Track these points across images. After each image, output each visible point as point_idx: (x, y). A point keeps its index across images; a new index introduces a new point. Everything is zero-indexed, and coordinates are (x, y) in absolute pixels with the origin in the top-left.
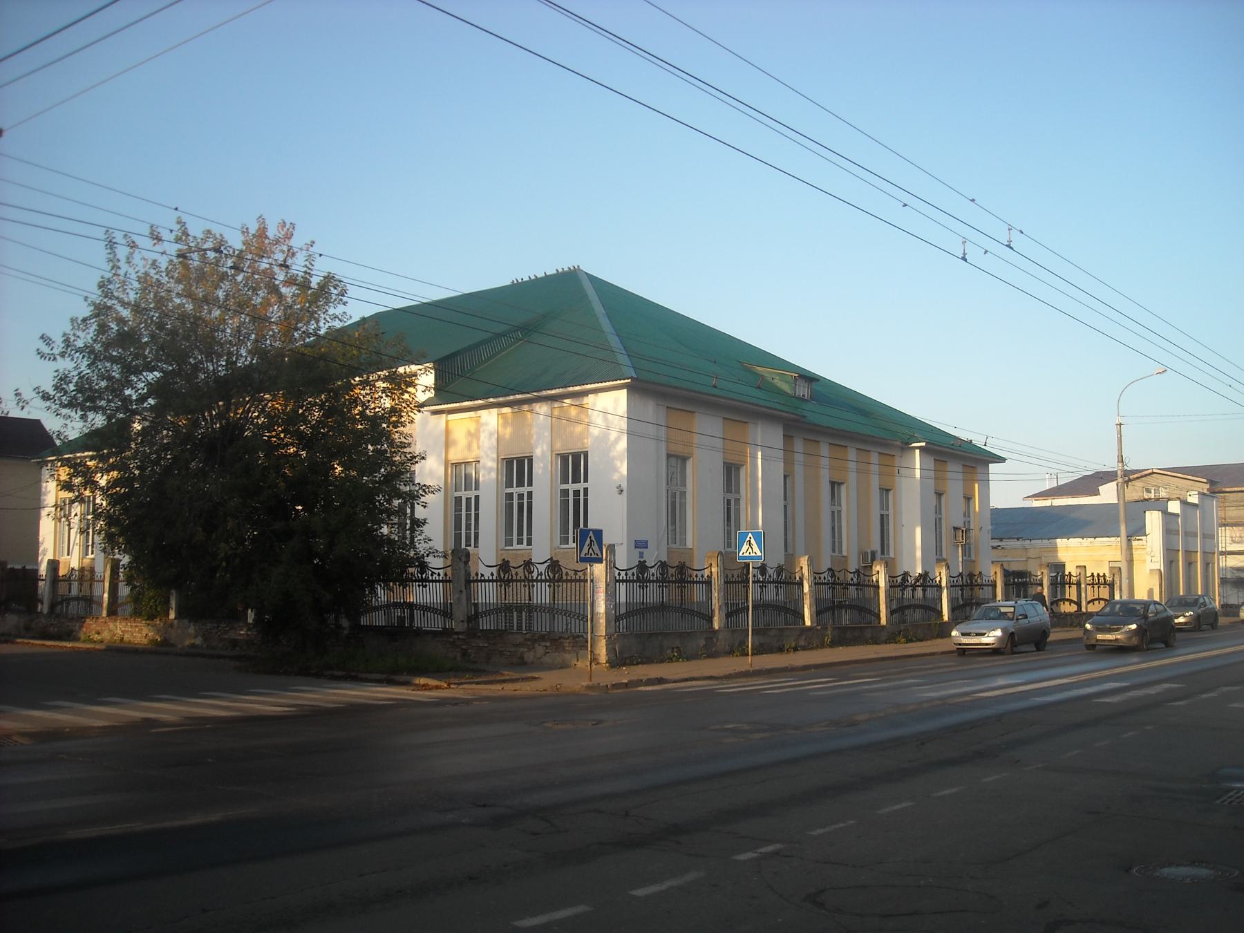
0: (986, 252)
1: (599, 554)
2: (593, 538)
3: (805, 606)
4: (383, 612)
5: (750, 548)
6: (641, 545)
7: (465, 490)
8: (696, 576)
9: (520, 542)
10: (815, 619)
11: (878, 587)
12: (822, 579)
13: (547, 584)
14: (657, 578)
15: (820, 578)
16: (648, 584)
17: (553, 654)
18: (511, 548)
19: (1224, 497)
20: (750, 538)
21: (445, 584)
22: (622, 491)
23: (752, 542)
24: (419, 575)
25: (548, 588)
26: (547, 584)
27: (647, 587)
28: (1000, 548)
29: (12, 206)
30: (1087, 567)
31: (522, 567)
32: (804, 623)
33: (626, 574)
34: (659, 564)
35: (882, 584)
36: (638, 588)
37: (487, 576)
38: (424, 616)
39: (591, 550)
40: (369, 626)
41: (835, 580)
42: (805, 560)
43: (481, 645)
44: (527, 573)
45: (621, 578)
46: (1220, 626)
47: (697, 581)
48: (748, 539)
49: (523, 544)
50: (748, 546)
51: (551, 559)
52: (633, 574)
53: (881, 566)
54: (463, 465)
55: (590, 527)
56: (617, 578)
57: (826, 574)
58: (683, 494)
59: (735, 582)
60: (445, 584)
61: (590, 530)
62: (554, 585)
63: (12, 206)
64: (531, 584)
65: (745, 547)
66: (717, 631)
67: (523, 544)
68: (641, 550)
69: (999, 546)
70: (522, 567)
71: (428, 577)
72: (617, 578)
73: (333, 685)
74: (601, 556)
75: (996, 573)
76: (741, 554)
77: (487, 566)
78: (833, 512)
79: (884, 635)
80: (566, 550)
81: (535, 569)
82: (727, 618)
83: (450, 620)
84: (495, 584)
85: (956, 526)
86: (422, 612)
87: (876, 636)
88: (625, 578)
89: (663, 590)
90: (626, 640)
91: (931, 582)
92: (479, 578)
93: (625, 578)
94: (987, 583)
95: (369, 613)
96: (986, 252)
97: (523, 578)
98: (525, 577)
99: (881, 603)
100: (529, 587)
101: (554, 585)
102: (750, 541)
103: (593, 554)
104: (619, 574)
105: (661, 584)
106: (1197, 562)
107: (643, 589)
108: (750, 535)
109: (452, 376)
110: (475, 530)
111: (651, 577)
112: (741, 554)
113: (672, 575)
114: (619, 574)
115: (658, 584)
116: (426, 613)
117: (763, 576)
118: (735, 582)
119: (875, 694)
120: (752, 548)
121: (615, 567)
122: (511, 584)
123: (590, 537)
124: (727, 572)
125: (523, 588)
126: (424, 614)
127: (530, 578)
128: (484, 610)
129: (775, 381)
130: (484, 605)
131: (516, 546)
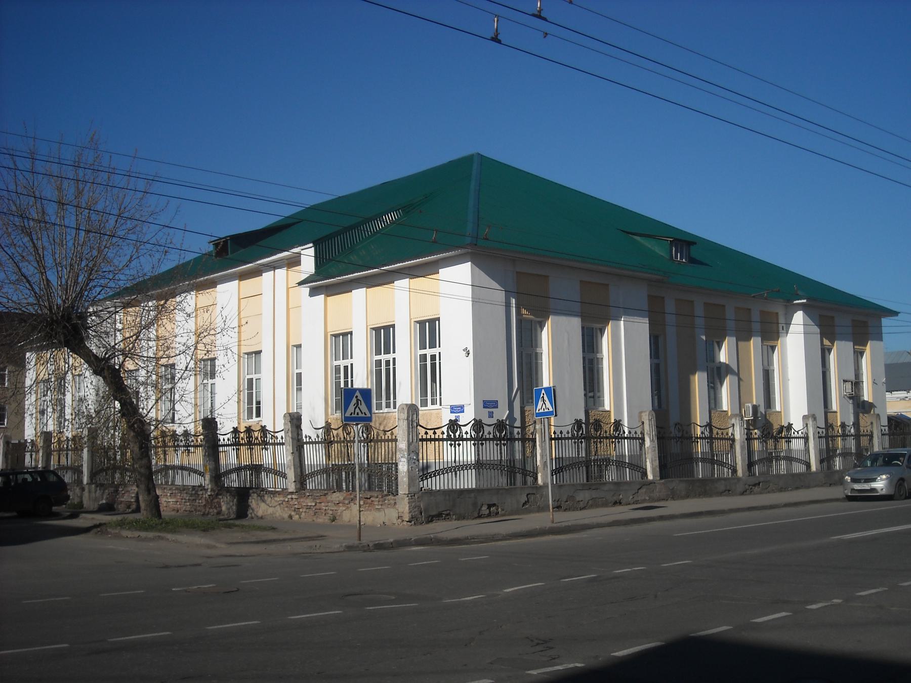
3: (648, 460)
4: (236, 473)
5: (544, 404)
6: (489, 405)
7: (343, 359)
8: (722, 434)
9: (388, 406)
10: (658, 474)
11: (733, 440)
12: (226, 440)
13: (473, 442)
14: (471, 436)
15: (722, 434)
16: (253, 447)
17: (365, 513)
18: (381, 411)
19: (185, 253)
20: (543, 394)
21: (724, 441)
22: (468, 354)
23: (545, 398)
24: (234, 440)
25: (473, 447)
26: (473, 442)
27: (459, 445)
28: (907, 399)
30: (880, 414)
31: (341, 428)
32: (647, 477)
33: (435, 433)
34: (473, 422)
35: (737, 436)
36: (707, 444)
37: (314, 437)
38: (267, 478)
39: (357, 408)
40: (238, 487)
41: (239, 441)
42: (646, 415)
43: (309, 504)
44: (345, 434)
45: (556, 436)
47: (636, 437)
48: (542, 395)
50: (542, 402)
51: (474, 419)
52: (443, 433)
53: (736, 419)
54: (341, 337)
55: (355, 386)
56: (553, 436)
57: (228, 436)
59: (565, 439)
60: (629, 440)
61: (356, 390)
62: (478, 443)
64: (349, 444)
65: (540, 403)
66: (541, 486)
68: (491, 410)
69: (907, 397)
70: (341, 428)
71: (463, 436)
72: (553, 436)
74: (370, 416)
75: (872, 423)
76: (537, 411)
77: (315, 429)
78: (351, 358)
79: (740, 488)
80: (425, 412)
81: (352, 430)
82: (821, 463)
83: (621, 468)
84: (570, 441)
85: (845, 379)
86: (265, 473)
87: (729, 488)
88: (281, 442)
89: (501, 449)
90: (432, 498)
91: (796, 433)
92: (308, 440)
93: (281, 442)
94: (720, 436)
95: (231, 474)
97: (342, 439)
98: (344, 438)
99: (737, 455)
100: (368, 447)
101: (367, 444)
102: (543, 397)
103: (360, 413)
104: (426, 433)
105: (453, 443)
107: (455, 447)
108: (543, 391)
109: (323, 261)
111: (271, 440)
112: (537, 411)
113: (489, 433)
114: (426, 433)
115: (573, 441)
116: (268, 474)
117: (787, 432)
118: (565, 439)
120: (545, 404)
121: (418, 424)
122: (333, 445)
123: (357, 397)
124: (882, 427)
125: (362, 448)
126: (267, 475)
127: (348, 439)
128: (313, 471)
130: (315, 466)
131: (430, 406)
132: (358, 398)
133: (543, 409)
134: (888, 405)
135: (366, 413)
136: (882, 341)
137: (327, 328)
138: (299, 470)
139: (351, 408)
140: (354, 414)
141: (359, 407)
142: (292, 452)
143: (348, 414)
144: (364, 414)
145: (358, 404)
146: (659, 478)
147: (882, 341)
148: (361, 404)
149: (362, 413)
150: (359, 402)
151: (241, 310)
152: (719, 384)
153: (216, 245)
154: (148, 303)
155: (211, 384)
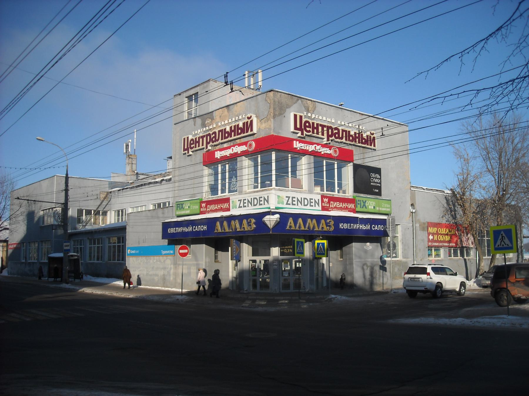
0: (11, 168)
1: (323, 252)
2: (504, 235)
29: (113, 34)
39: (502, 242)
46: (240, 247)
48: (320, 246)
49: (317, 243)
58: (114, 217)
63: (113, 34)
67: (317, 243)
68: (503, 247)
73: (149, 294)
96: (11, 168)
102: (321, 247)
103: (504, 245)
106: (510, 262)
110: (119, 218)
112: (297, 251)
119: (416, 279)
123: (502, 234)
129: (94, 292)
132: (503, 235)
133: (502, 245)
134: (326, 132)
135: (509, 245)
136: (162, 239)
137: (202, 140)
138: (314, 255)
139: (499, 242)
140: (501, 245)
141: (504, 241)
142: (313, 2)
143: (496, 246)
144: (507, 245)
145: (503, 239)
146: (167, 244)
147: (162, 239)
148: (505, 239)
149: (506, 245)
150: (504, 238)
151: (102, 204)
152: (210, 151)
153: (342, 280)
154: (203, 129)
155: (6, 241)
